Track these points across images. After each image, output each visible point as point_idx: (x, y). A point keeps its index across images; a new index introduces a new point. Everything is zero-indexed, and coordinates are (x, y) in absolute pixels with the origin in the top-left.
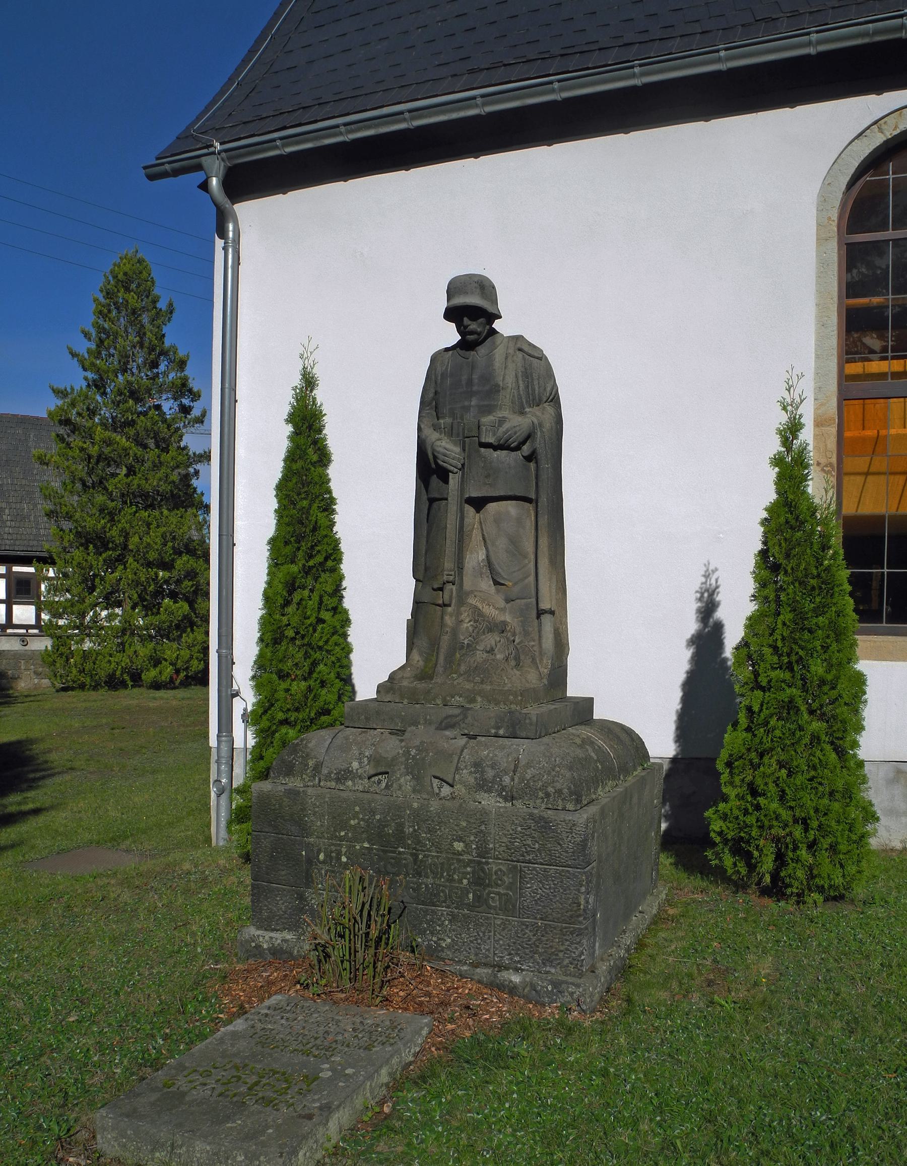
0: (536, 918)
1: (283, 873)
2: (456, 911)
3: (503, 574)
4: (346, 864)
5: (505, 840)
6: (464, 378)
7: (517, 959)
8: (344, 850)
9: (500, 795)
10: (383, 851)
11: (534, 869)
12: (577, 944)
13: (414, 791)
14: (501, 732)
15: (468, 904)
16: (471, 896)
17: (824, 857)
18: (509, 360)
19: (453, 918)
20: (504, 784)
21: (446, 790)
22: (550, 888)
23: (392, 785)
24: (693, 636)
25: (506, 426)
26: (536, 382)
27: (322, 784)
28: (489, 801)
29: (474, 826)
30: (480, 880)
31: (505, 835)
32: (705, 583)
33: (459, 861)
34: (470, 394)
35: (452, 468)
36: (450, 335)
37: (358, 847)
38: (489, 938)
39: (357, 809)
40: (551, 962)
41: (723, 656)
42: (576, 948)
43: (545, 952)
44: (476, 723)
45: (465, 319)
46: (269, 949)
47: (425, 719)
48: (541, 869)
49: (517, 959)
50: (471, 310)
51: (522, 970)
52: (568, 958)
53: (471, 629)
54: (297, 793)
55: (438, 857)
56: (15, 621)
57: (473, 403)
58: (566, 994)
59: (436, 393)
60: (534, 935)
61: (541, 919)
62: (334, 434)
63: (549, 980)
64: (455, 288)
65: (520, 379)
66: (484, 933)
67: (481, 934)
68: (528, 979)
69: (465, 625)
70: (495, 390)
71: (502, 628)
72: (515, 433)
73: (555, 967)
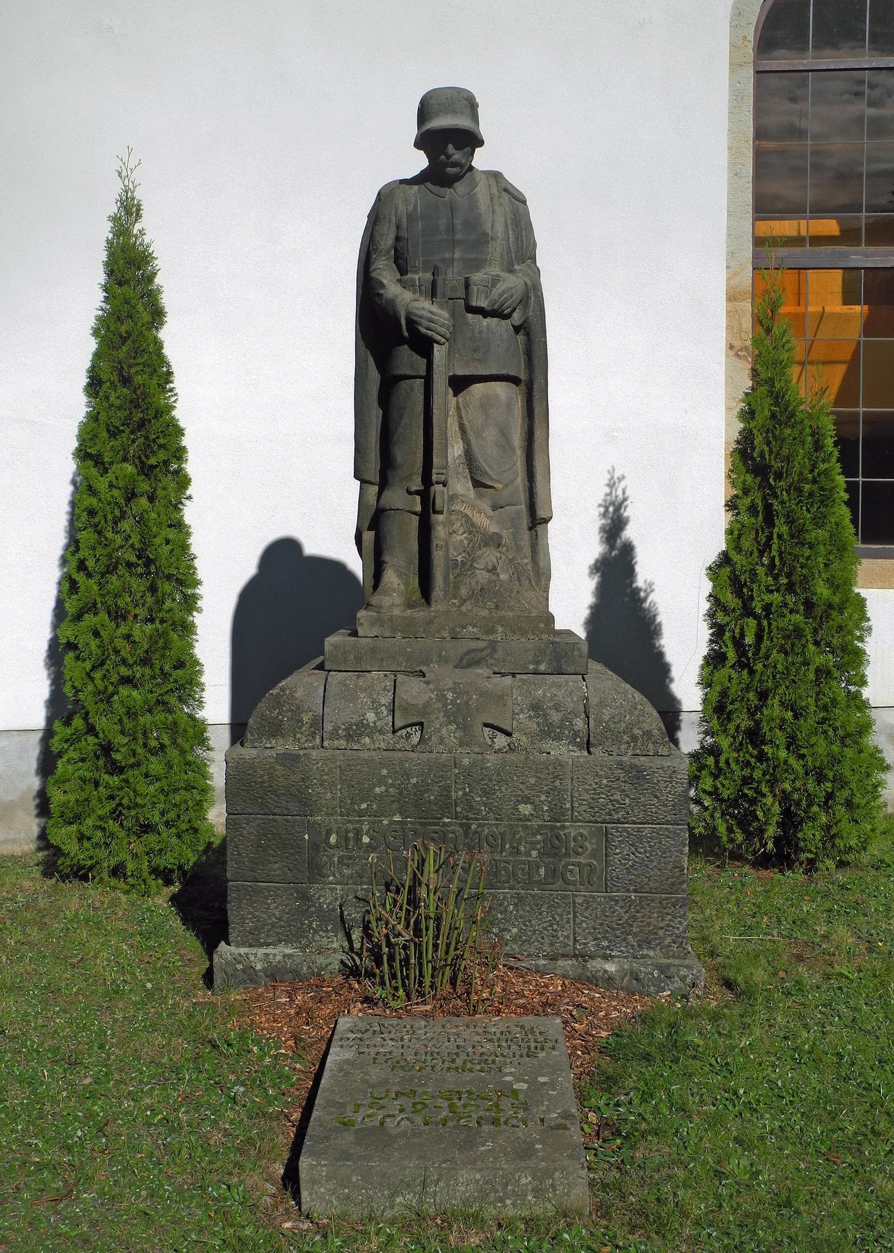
0: (628, 891)
1: (276, 866)
2: (523, 892)
3: (490, 473)
4: (369, 846)
5: (586, 796)
6: (443, 223)
7: (605, 943)
8: (365, 828)
9: (574, 743)
10: (421, 824)
11: (625, 829)
12: (681, 917)
13: (461, 744)
14: (542, 667)
15: (539, 882)
16: (542, 871)
17: (841, 811)
18: (496, 201)
19: (520, 901)
20: (576, 728)
21: (501, 740)
22: (645, 852)
23: (430, 739)
24: (597, 561)
25: (501, 287)
26: (524, 233)
27: (326, 744)
29: (545, 782)
30: (554, 848)
31: (587, 791)
32: (610, 494)
33: (526, 828)
34: (454, 244)
35: (439, 338)
37: (385, 822)
38: (568, 922)
39: (384, 772)
40: (649, 943)
41: (634, 585)
42: (680, 923)
43: (641, 931)
44: (509, 659)
45: (450, 146)
46: (264, 970)
47: (440, 656)
48: (633, 829)
49: (605, 943)
50: (448, 135)
51: (612, 957)
52: (670, 935)
53: (466, 542)
54: (295, 758)
55: (497, 826)
57: (456, 256)
58: (677, 979)
59: (398, 239)
60: (626, 912)
61: (635, 891)
62: (172, 284)
63: (652, 964)
65: (510, 227)
66: (561, 916)
67: (557, 918)
68: (626, 967)
69: (459, 538)
70: (483, 240)
71: (494, 541)
72: (512, 297)
73: (654, 949)
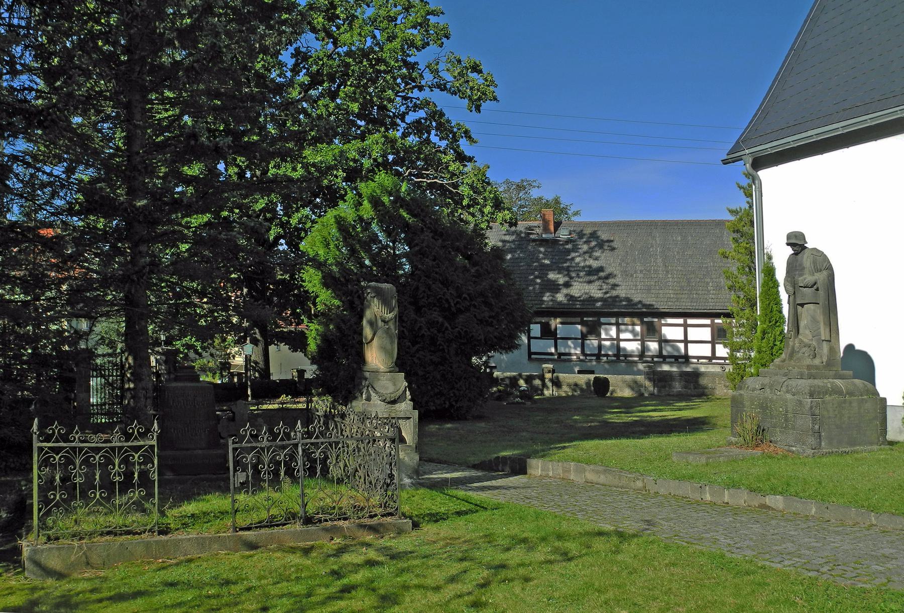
28: (789, 396)
36: (790, 251)
56: (718, 355)
64: (789, 236)
